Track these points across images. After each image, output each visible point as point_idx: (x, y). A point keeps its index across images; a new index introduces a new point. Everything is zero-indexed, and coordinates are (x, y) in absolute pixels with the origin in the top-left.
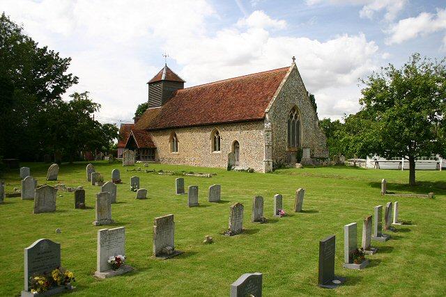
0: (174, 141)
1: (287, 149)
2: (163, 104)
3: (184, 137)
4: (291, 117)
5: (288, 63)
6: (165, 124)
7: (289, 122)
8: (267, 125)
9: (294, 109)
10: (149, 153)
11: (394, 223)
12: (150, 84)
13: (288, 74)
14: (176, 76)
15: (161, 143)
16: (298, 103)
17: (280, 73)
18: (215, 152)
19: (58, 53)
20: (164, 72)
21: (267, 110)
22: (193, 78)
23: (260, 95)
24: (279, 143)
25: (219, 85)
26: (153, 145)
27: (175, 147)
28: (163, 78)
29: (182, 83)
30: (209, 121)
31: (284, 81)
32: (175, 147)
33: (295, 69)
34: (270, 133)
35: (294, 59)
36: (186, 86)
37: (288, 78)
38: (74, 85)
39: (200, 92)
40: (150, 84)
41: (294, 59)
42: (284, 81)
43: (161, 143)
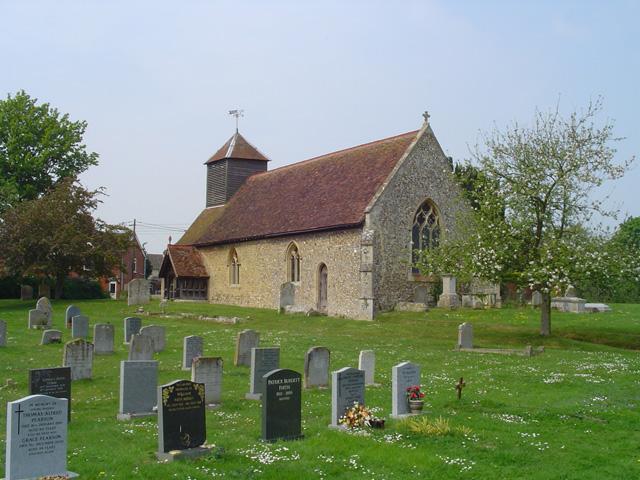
0: (234, 264)
1: (411, 278)
2: (228, 199)
3: (247, 253)
4: (421, 220)
5: (416, 125)
6: (222, 236)
7: (415, 231)
8: (368, 232)
9: (426, 206)
10: (198, 285)
11: (334, 424)
12: (209, 164)
13: (413, 144)
14: (253, 150)
15: (215, 264)
16: (434, 195)
17: (406, 139)
18: (233, 285)
19: (66, 116)
20: (233, 143)
21: (367, 208)
22: (282, 152)
23: (367, 181)
24: (395, 266)
25: (327, 162)
26: (205, 273)
27: (235, 278)
28: (228, 155)
29: (262, 163)
30: (282, 230)
31: (406, 155)
32: (235, 278)
33: (428, 136)
34: (371, 249)
35: (426, 116)
36: (271, 166)
37: (414, 149)
38: (91, 167)
39: (288, 175)
40: (209, 164)
41: (426, 116)
42: (406, 155)
43: (215, 264)
